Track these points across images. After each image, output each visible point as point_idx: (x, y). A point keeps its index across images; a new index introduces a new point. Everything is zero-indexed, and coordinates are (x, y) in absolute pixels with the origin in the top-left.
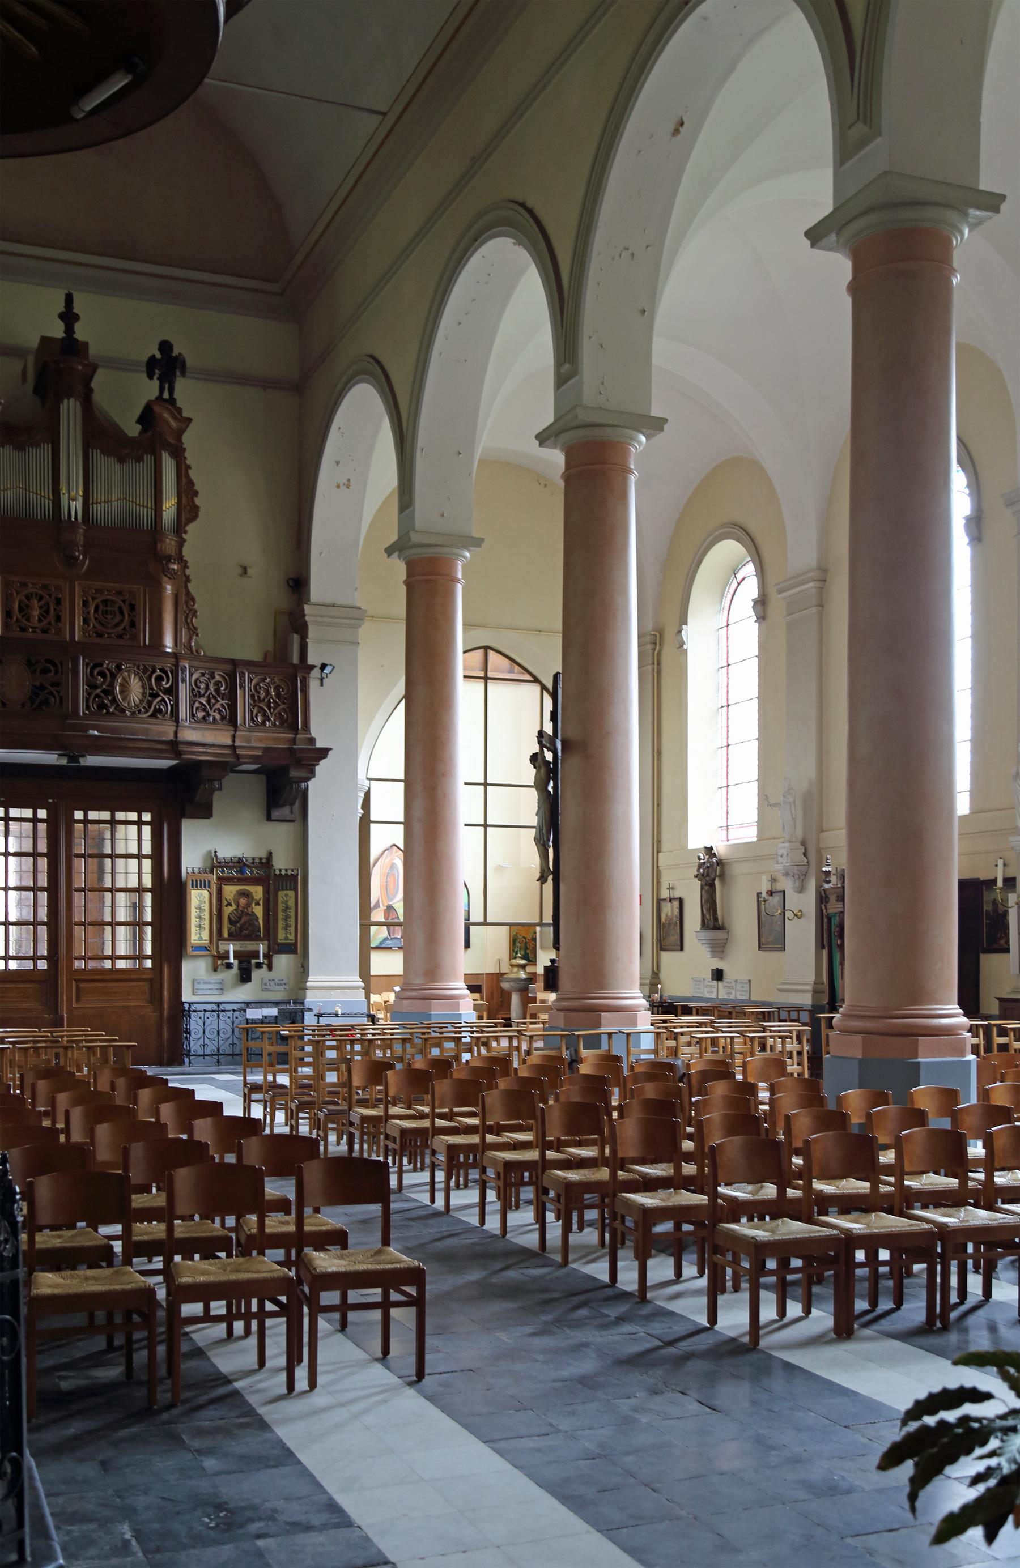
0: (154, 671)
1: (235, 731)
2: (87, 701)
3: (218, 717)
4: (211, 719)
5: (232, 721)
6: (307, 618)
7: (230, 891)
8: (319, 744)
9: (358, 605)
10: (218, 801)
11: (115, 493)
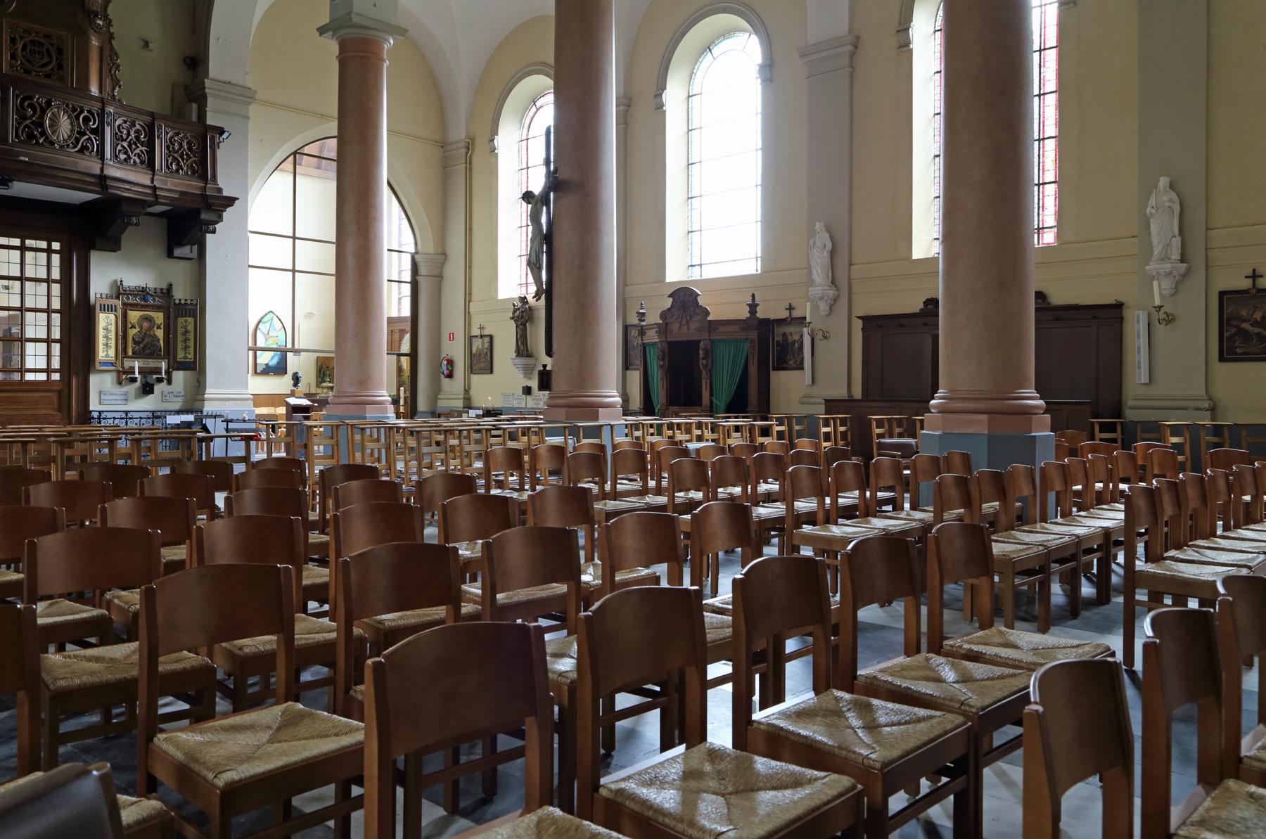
0: (82, 112)
2: (17, 129)
5: (151, 165)
7: (134, 316)
8: (225, 194)
10: (126, 239)
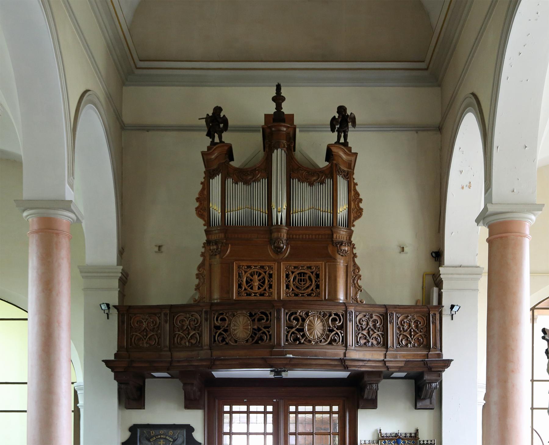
0: (330, 315)
1: (387, 351)
2: (287, 336)
3: (375, 343)
4: (370, 344)
5: (385, 345)
6: (441, 276)
8: (445, 358)
9: (478, 265)
11: (308, 205)
